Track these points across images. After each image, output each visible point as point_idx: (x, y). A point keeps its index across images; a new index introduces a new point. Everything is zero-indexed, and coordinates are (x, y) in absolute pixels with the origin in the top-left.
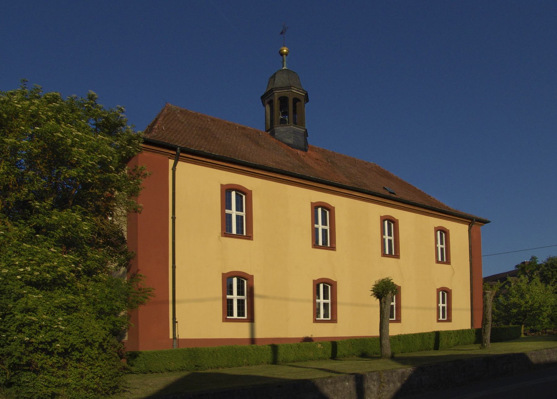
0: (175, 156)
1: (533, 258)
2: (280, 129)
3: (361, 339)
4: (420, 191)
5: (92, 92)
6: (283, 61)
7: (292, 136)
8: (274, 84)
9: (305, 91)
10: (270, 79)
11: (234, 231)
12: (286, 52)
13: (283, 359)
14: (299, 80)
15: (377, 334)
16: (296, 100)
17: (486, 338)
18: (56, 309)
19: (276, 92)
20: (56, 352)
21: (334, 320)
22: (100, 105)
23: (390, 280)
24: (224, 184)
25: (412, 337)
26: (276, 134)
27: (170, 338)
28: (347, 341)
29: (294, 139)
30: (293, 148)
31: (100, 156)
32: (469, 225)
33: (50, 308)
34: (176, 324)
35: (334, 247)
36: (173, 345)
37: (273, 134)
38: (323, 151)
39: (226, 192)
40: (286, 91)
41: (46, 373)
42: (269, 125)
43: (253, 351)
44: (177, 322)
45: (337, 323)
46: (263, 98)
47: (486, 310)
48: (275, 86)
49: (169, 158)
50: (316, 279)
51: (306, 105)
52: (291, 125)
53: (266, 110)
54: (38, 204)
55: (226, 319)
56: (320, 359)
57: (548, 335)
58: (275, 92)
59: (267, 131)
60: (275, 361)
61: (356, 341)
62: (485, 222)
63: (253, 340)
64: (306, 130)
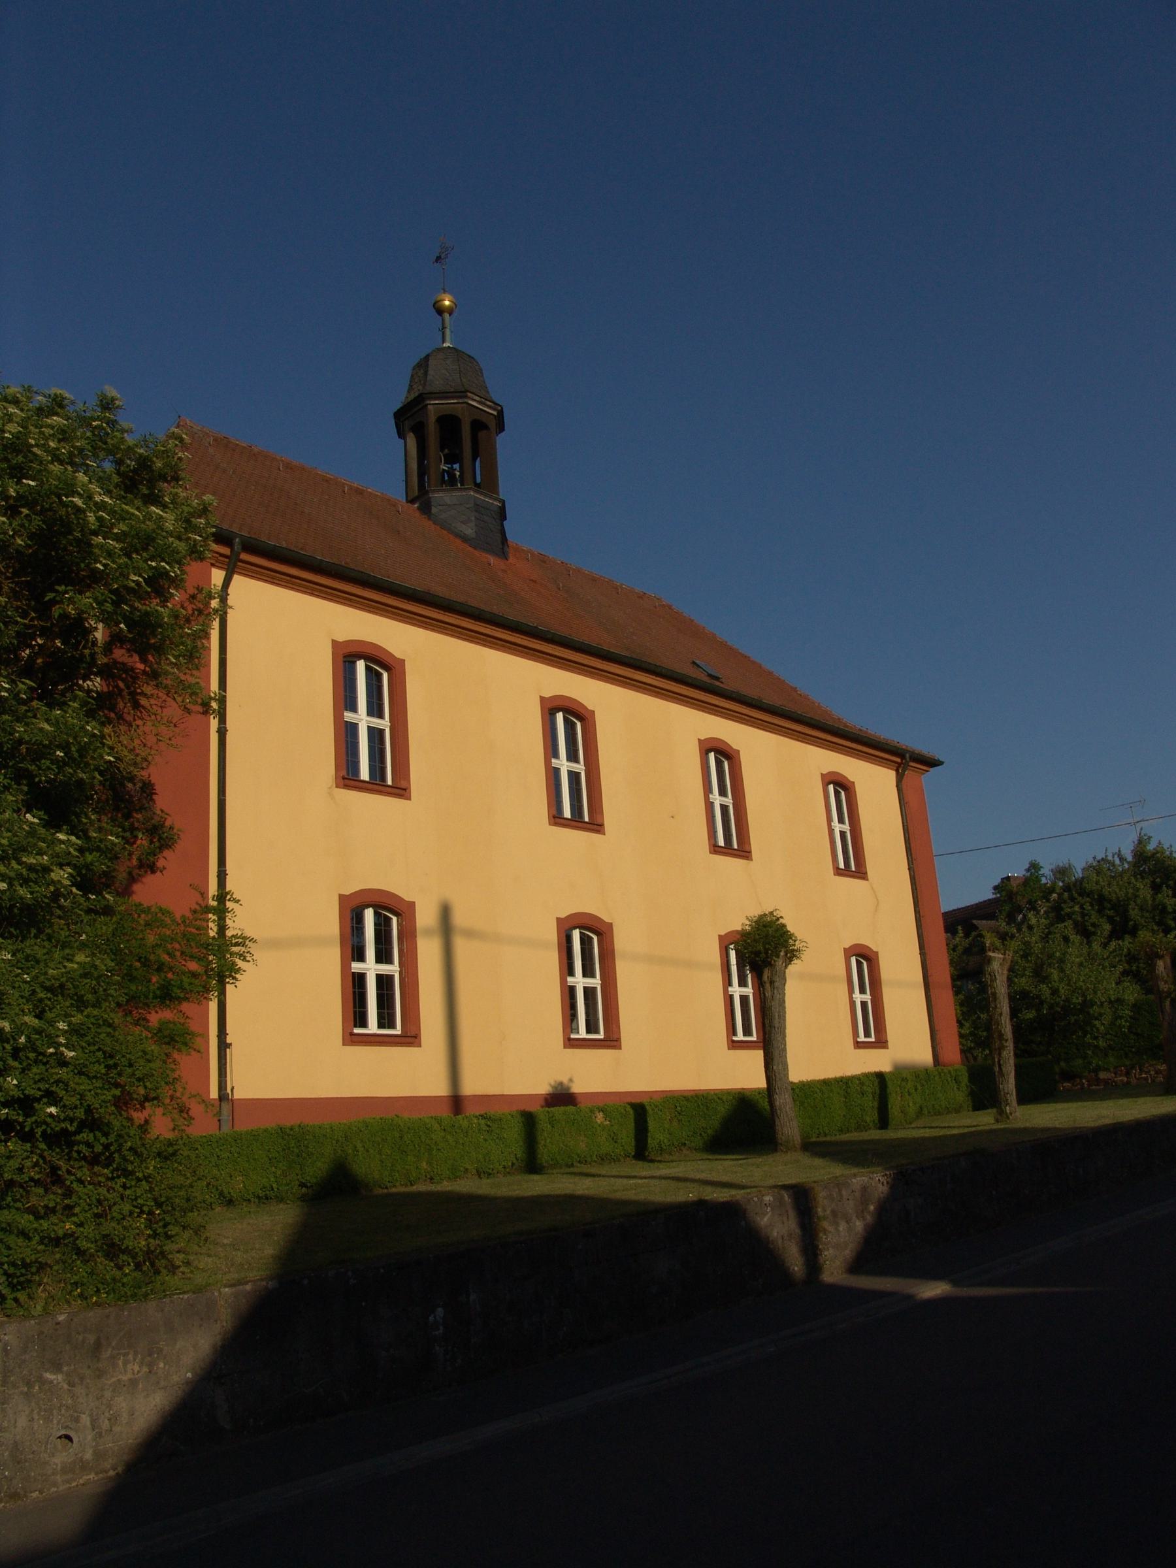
0: (227, 560)
1: (1034, 867)
2: (442, 497)
3: (696, 1096)
4: (771, 673)
5: (111, 392)
6: (444, 328)
7: (473, 518)
8: (425, 384)
9: (498, 405)
10: (414, 369)
11: (365, 774)
12: (449, 306)
13: (515, 1161)
14: (483, 376)
15: (762, 1083)
16: (478, 426)
17: (1006, 1091)
18: (49, 995)
19: (432, 402)
20: (39, 1131)
21: (612, 1041)
22: (125, 425)
23: (778, 919)
24: (341, 640)
25: (821, 1091)
26: (434, 510)
27: (211, 1097)
28: (664, 1102)
29: (476, 525)
30: (475, 548)
31: (154, 564)
32: (897, 771)
33: (34, 992)
34: (228, 1050)
35: (599, 822)
36: (219, 1120)
37: (426, 509)
38: (543, 560)
39: (345, 662)
40: (455, 401)
41: (10, 1203)
42: (416, 488)
43: (443, 1134)
44: (231, 1044)
45: (619, 1047)
46: (400, 416)
47: (996, 1006)
48: (429, 389)
49: (213, 565)
50: (563, 915)
51: (498, 438)
52: (470, 489)
53: (408, 448)
54: (7, 686)
55: (352, 1034)
56: (603, 1159)
57: (1102, 1087)
58: (428, 402)
59: (412, 501)
60: (532, 1165)
61: (685, 1102)
62: (932, 763)
63: (457, 1102)
64: (503, 502)
